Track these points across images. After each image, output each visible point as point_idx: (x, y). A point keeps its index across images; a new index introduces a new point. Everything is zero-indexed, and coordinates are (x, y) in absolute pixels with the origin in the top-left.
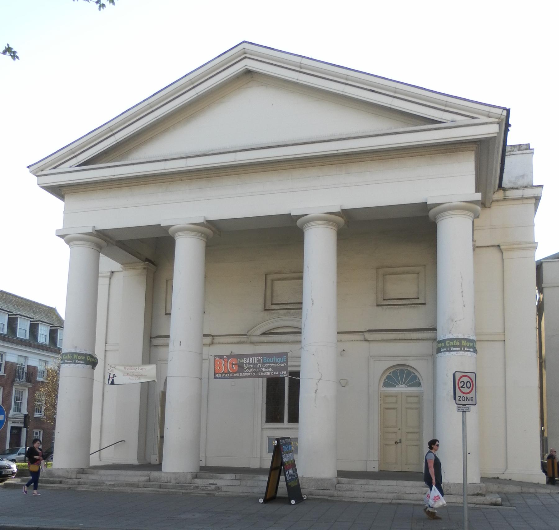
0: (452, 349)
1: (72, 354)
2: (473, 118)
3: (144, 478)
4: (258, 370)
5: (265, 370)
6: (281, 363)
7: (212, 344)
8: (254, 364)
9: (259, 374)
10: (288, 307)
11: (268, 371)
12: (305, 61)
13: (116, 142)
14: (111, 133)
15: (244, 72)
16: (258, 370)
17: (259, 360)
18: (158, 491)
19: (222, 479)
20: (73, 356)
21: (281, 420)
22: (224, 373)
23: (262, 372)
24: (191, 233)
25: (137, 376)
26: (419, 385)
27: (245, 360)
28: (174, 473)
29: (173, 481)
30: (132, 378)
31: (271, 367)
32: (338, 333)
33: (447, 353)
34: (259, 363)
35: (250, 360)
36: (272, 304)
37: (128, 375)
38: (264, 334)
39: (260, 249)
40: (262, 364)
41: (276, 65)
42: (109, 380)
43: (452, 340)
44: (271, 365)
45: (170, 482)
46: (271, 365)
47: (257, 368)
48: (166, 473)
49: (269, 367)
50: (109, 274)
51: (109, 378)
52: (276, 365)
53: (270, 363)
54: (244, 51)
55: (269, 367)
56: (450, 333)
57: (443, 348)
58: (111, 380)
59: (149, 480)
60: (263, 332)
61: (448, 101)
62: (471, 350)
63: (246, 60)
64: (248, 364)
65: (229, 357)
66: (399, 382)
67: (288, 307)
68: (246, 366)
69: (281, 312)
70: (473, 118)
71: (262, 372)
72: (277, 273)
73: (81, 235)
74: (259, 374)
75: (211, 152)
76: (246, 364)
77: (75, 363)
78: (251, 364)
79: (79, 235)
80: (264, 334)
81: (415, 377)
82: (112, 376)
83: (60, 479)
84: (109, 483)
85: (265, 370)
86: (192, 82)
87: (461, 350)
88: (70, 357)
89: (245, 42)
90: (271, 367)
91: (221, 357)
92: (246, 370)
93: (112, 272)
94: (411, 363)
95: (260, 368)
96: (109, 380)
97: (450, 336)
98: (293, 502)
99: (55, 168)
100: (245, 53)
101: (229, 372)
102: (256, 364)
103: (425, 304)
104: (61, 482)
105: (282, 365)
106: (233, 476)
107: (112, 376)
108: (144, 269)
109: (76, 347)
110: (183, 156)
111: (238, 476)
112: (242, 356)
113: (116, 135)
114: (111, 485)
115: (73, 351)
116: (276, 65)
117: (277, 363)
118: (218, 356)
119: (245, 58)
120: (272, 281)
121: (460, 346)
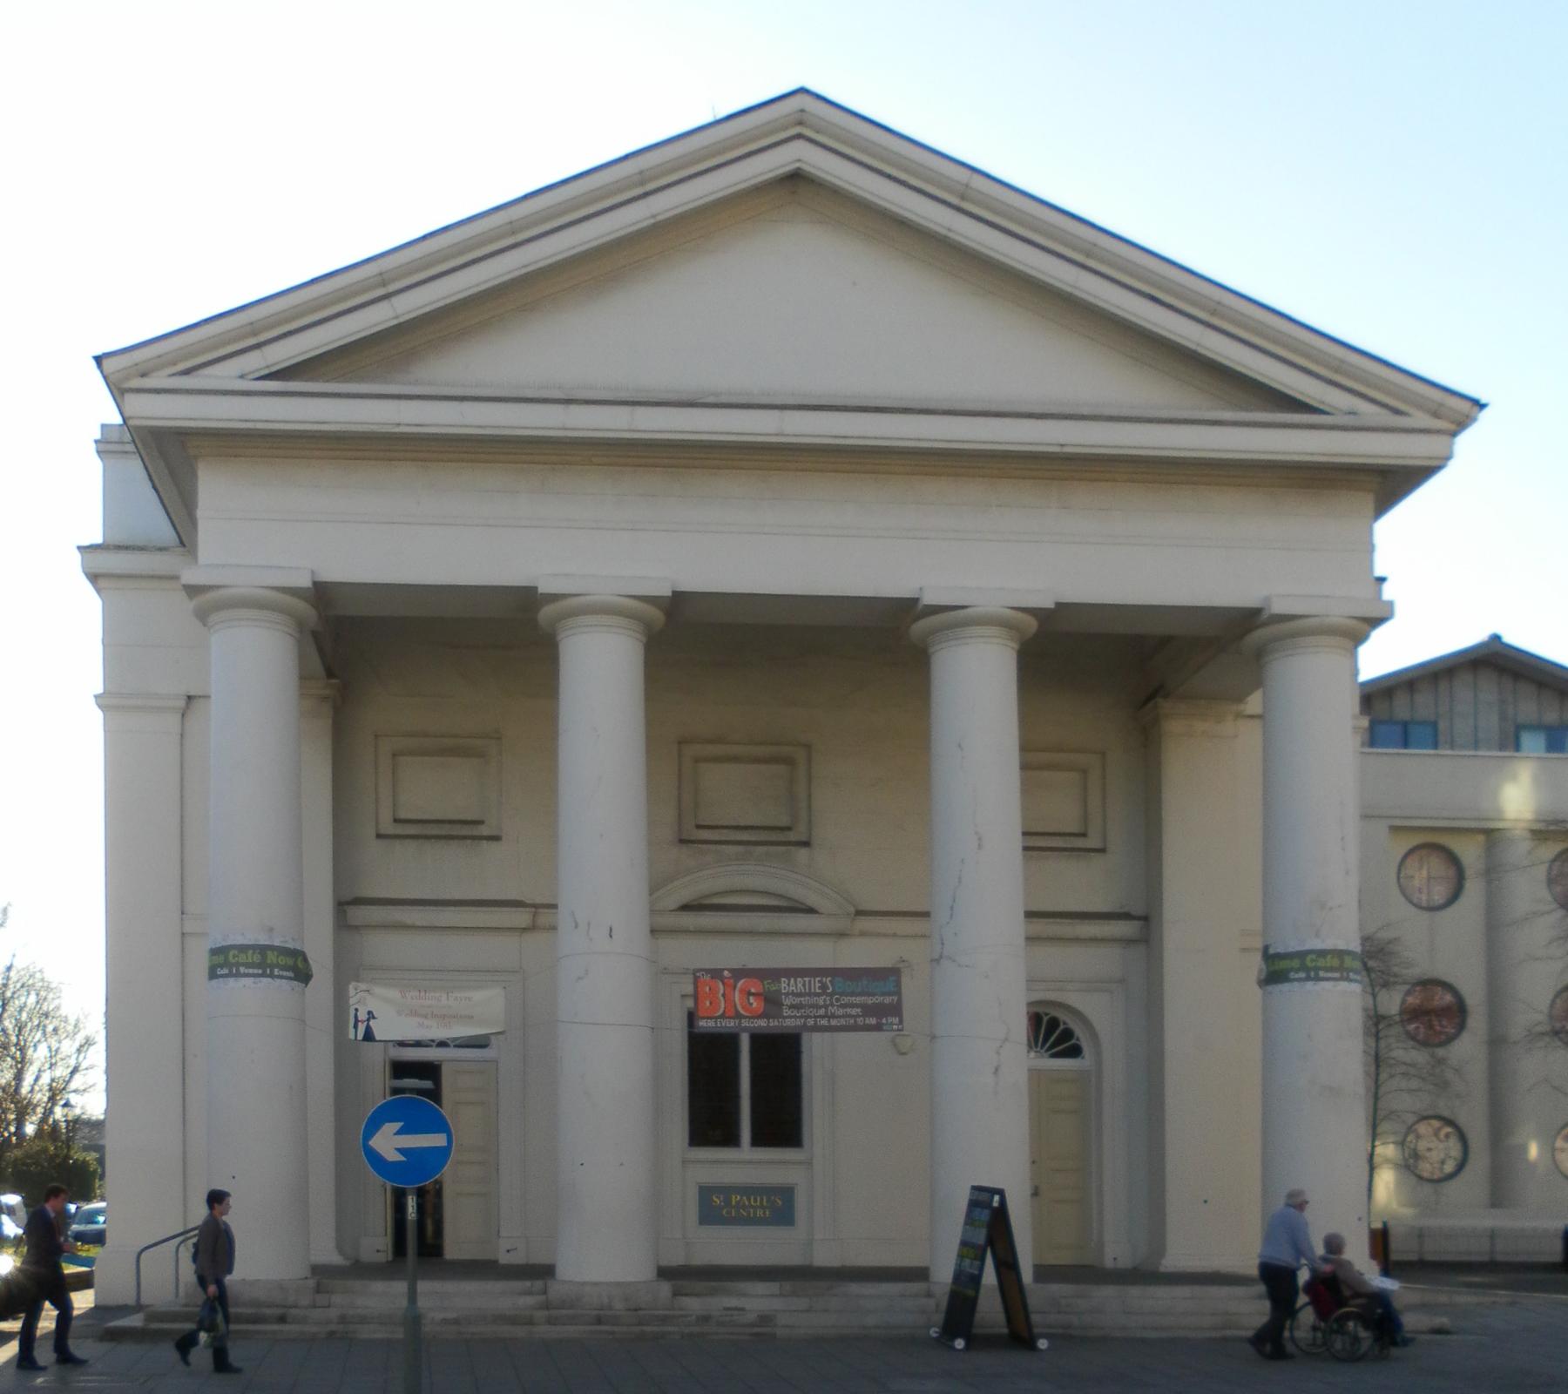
0: (1322, 974)
1: (263, 949)
2: (1397, 412)
3: (530, 1300)
4: (822, 1012)
5: (841, 1012)
6: (883, 994)
7: (533, 928)
8: (810, 994)
9: (824, 1022)
10: (745, 836)
11: (850, 1016)
12: (978, 182)
13: (395, 322)
14: (381, 292)
15: (799, 174)
16: (822, 1012)
17: (824, 987)
18: (613, 1333)
19: (744, 1295)
20: (264, 957)
21: (731, 1140)
22: (723, 1016)
23: (833, 1016)
24: (623, 621)
25: (444, 1016)
26: (1075, 1052)
27: (785, 985)
28: (618, 1284)
29: (619, 1305)
30: (426, 1022)
31: (856, 1006)
32: (925, 915)
33: (1309, 985)
34: (824, 993)
35: (798, 985)
36: (699, 827)
37: (414, 1013)
38: (686, 908)
39: (781, 683)
40: (831, 995)
41: (889, 177)
42: (356, 1027)
43: (1322, 953)
44: (858, 1000)
45: (610, 1308)
46: (858, 1000)
47: (818, 1007)
48: (565, 1282)
49: (853, 1006)
50: (182, 703)
51: (357, 1021)
52: (870, 1001)
53: (853, 994)
54: (800, 115)
55: (853, 1006)
56: (1317, 935)
57: (1297, 970)
58: (362, 1029)
59: (547, 1306)
60: (684, 901)
61: (515, 217)
62: (1337, 975)
63: (800, 144)
64: (793, 994)
65: (739, 973)
66: (1045, 1040)
67: (745, 836)
68: (787, 1001)
69: (761, 849)
70: (1397, 412)
71: (833, 1016)
72: (711, 742)
73: (261, 591)
74: (824, 1022)
75: (711, 400)
76: (787, 994)
77: (271, 976)
78: (800, 995)
79: (261, 591)
80: (686, 908)
81: (1068, 1034)
82: (362, 1016)
83: (279, 1311)
84: (439, 1316)
85: (841, 1012)
86: (642, 177)
87: (1308, 979)
88: (257, 958)
89: (802, 91)
90: (856, 1006)
91: (716, 974)
92: (786, 1012)
93: (189, 697)
94: (1074, 999)
95: (826, 1007)
96: (356, 1027)
97: (1318, 945)
98: (960, 1344)
99: (187, 372)
100: (800, 123)
101: (738, 1016)
102: (818, 995)
103: (1102, 851)
104: (282, 1319)
105: (888, 1000)
106: (773, 1287)
107: (362, 1016)
108: (324, 698)
109: (271, 930)
110: (623, 396)
111: (788, 1286)
112: (775, 974)
113: (394, 300)
114: (445, 1321)
115: (264, 941)
116: (889, 177)
117: (873, 995)
118: (707, 971)
119: (799, 136)
120: (697, 760)
121: (1340, 969)
